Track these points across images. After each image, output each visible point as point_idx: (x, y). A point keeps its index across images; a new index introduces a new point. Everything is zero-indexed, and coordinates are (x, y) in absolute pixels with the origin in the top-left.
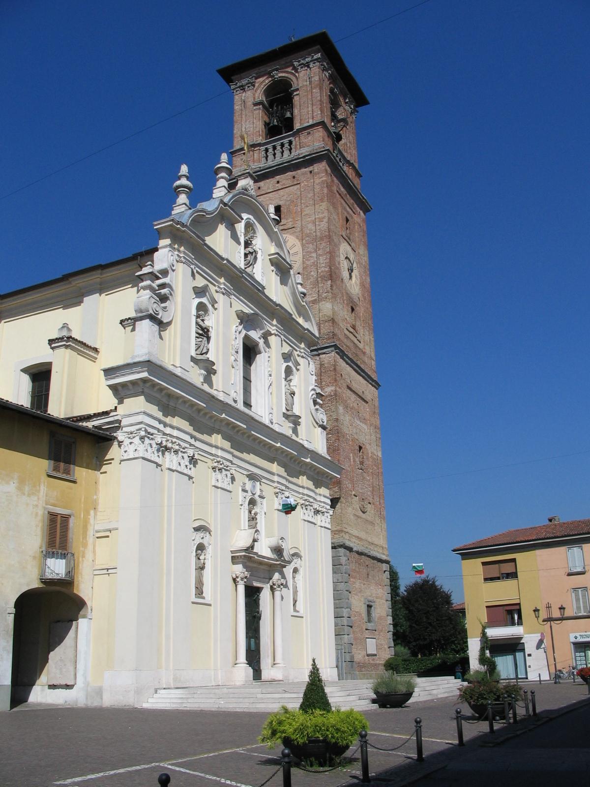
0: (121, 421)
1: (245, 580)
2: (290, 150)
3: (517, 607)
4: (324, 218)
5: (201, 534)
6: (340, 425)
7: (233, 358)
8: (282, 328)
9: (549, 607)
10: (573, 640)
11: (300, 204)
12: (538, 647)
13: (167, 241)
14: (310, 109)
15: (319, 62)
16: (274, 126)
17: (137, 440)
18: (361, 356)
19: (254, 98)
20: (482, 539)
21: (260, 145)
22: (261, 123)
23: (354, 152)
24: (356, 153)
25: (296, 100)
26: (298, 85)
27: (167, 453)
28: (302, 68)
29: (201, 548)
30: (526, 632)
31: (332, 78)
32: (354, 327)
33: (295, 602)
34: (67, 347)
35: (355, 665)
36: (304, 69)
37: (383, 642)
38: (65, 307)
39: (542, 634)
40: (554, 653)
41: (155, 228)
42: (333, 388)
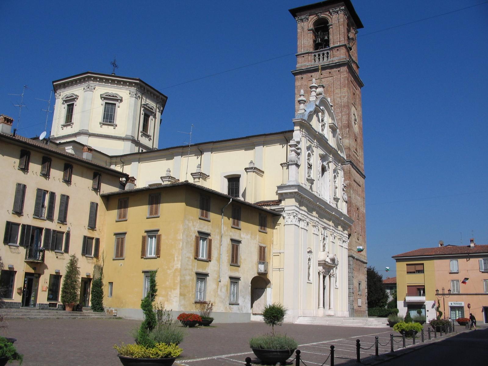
0: (284, 208)
1: (323, 273)
2: (328, 57)
3: (423, 287)
4: (345, 96)
5: (309, 254)
6: (351, 200)
7: (318, 176)
8: (334, 158)
9: (443, 289)
10: (450, 305)
11: (333, 87)
12: (433, 307)
13: (298, 128)
14: (338, 36)
15: (343, 11)
16: (319, 43)
17: (292, 217)
18: (359, 164)
19: (308, 27)
20: (406, 252)
21: (311, 53)
22: (312, 41)
23: (356, 55)
24: (357, 55)
25: (331, 30)
26: (332, 23)
27: (300, 221)
28: (334, 13)
29: (309, 259)
30: (427, 300)
31: (348, 18)
32: (356, 150)
33: (336, 281)
34: (254, 172)
35: (354, 311)
36: (335, 14)
37: (363, 301)
38: (246, 150)
39: (435, 301)
40: (444, 310)
41: (293, 121)
42: (349, 182)
